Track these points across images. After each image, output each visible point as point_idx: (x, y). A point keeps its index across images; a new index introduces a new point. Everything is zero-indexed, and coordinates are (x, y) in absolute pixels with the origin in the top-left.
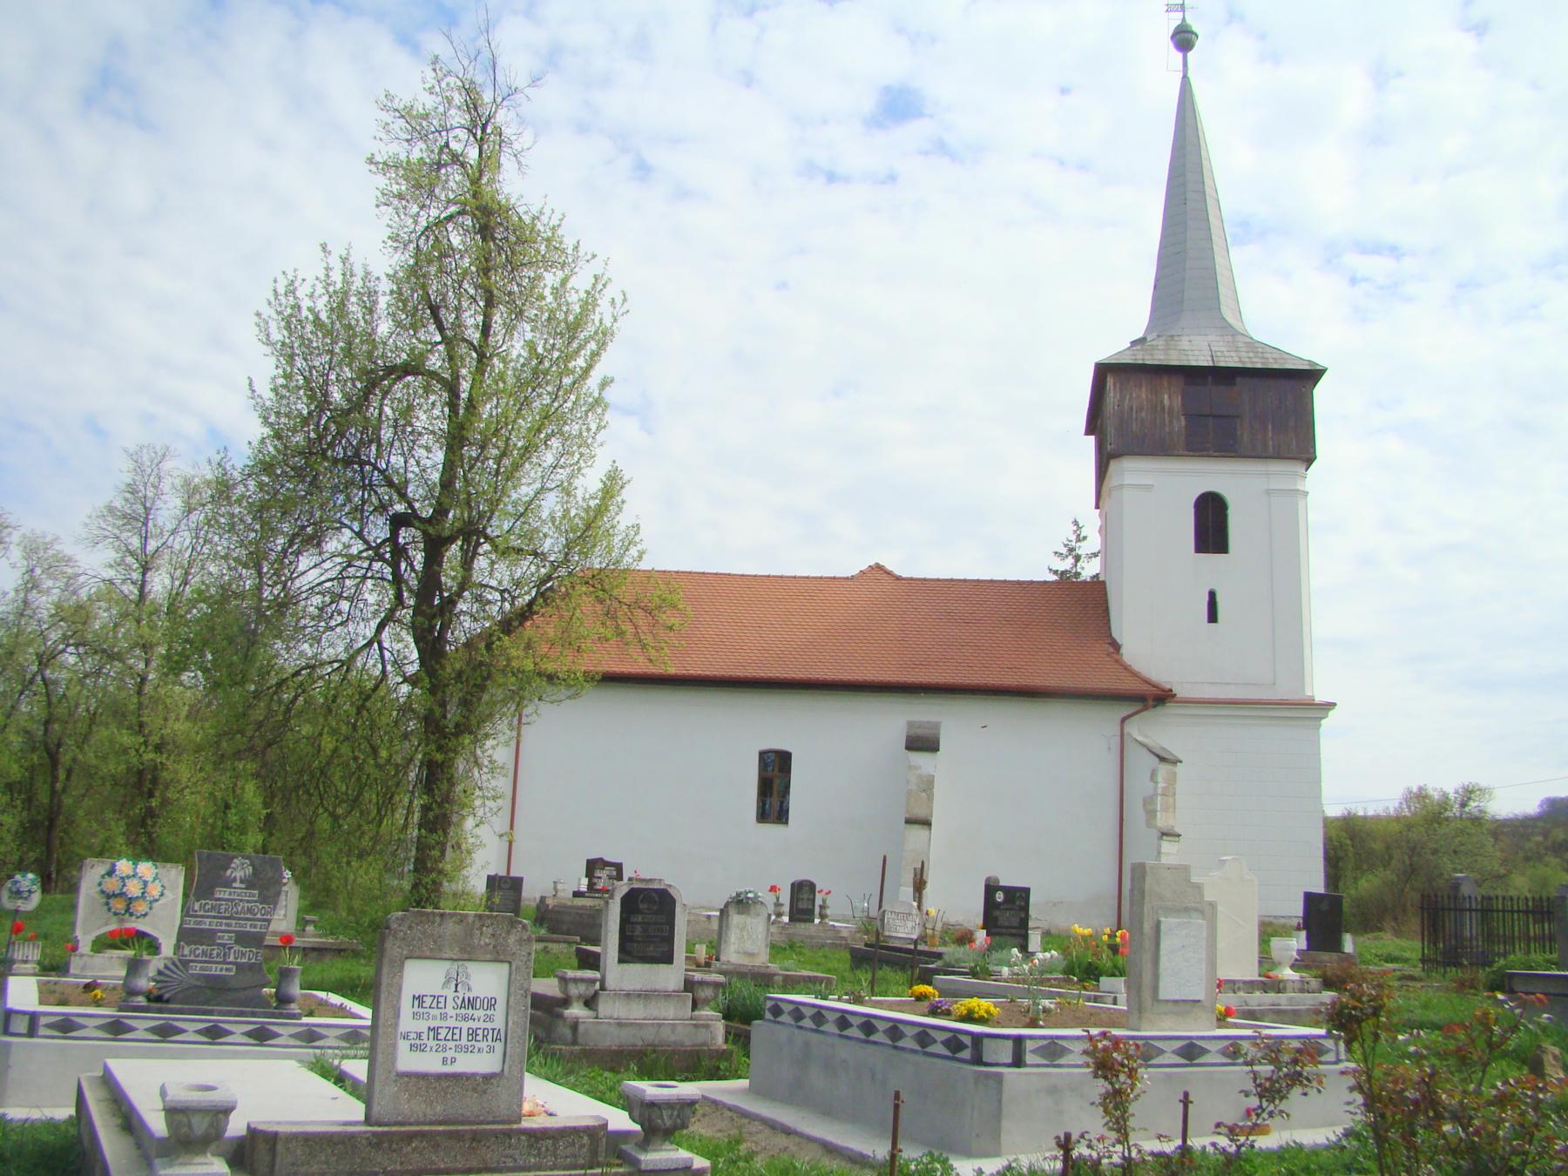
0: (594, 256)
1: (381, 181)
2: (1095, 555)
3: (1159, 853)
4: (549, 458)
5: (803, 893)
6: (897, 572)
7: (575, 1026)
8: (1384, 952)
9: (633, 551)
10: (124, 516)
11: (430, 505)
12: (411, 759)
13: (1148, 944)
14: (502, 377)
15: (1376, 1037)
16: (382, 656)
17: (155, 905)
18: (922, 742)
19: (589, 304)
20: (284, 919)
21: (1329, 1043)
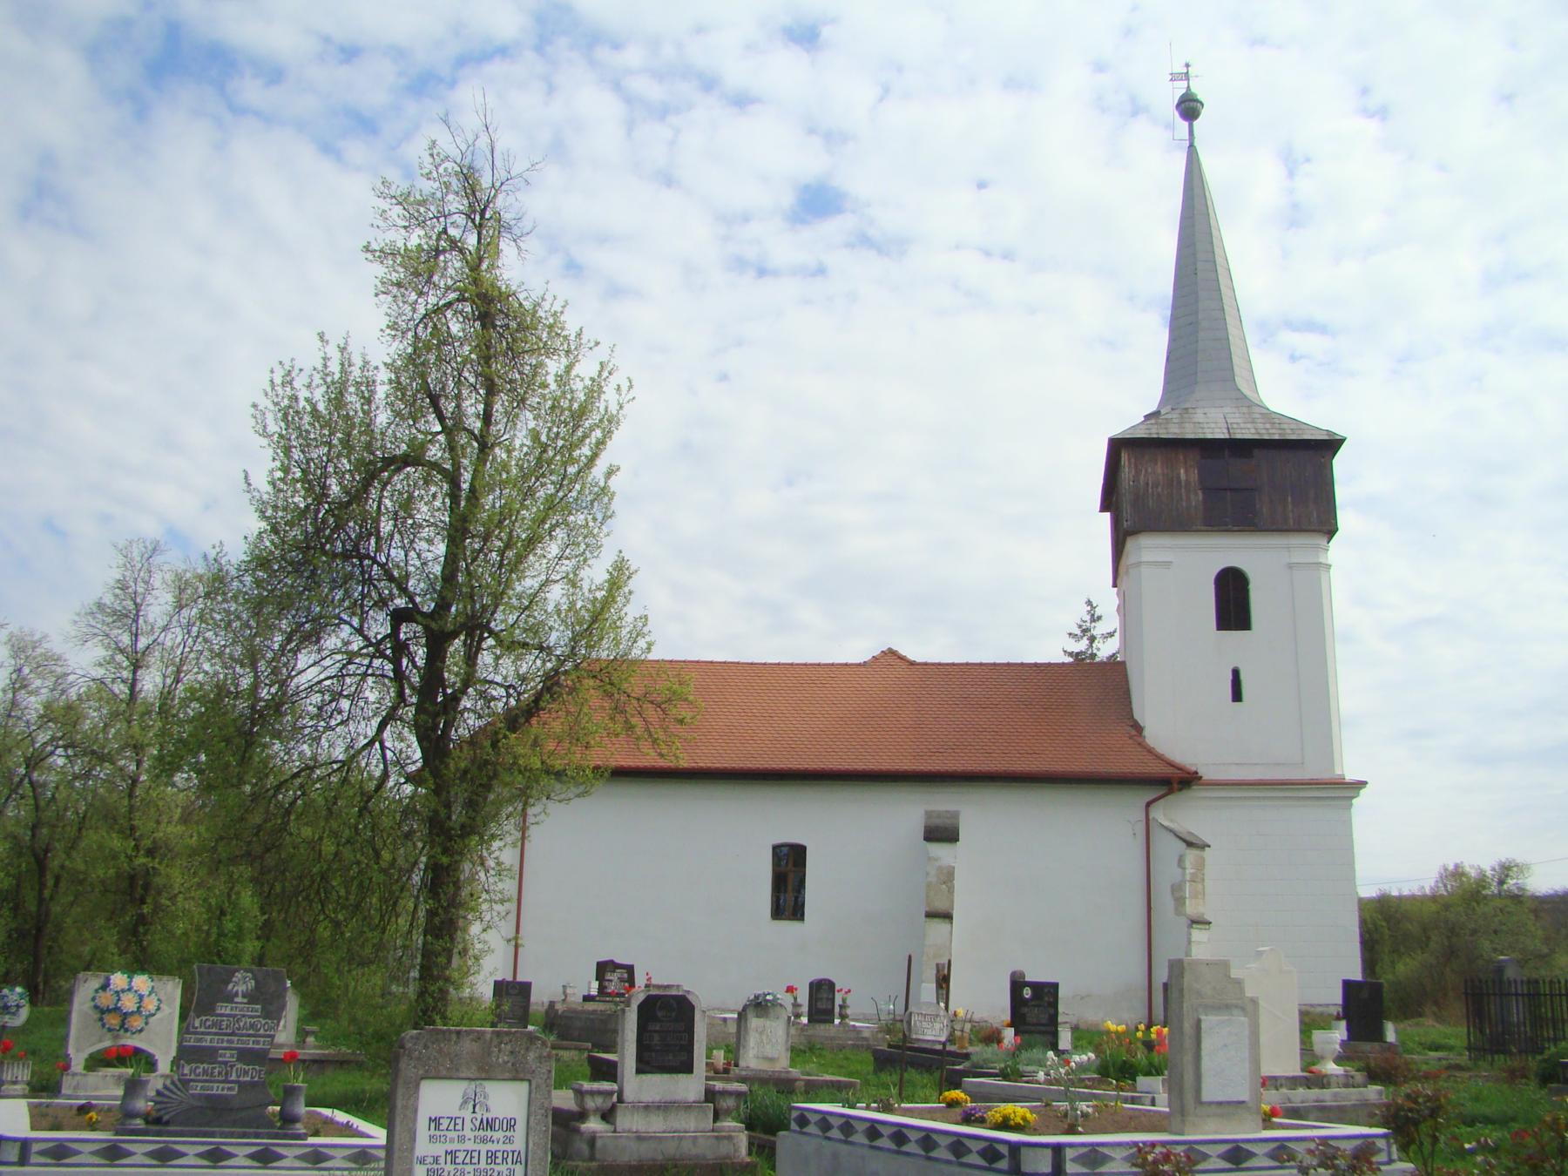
0: (597, 344)
1: (379, 270)
2: (1111, 635)
3: (1189, 942)
4: (554, 549)
5: (822, 991)
6: (911, 657)
7: (592, 1140)
8: (1428, 1039)
9: (642, 643)
10: (115, 612)
11: (432, 599)
12: (415, 863)
13: (1188, 1042)
14: (505, 467)
15: (1435, 1140)
16: (384, 756)
17: (152, 1020)
18: (941, 833)
19: (594, 391)
20: (285, 1034)
21: (1381, 1143)
